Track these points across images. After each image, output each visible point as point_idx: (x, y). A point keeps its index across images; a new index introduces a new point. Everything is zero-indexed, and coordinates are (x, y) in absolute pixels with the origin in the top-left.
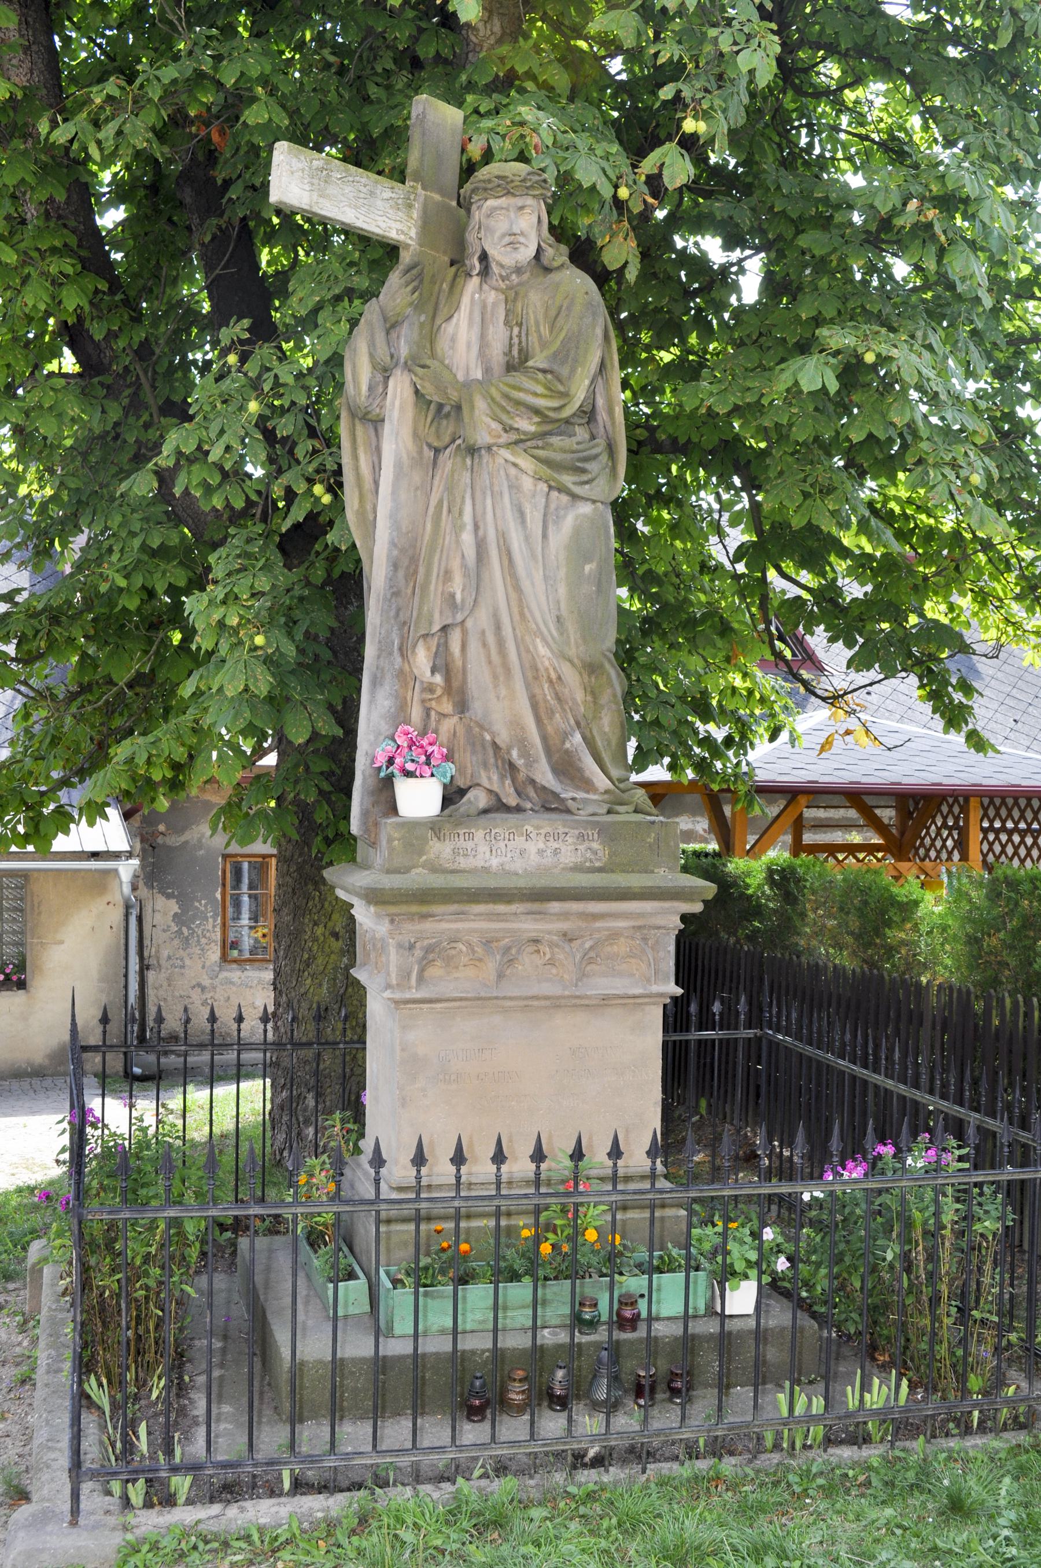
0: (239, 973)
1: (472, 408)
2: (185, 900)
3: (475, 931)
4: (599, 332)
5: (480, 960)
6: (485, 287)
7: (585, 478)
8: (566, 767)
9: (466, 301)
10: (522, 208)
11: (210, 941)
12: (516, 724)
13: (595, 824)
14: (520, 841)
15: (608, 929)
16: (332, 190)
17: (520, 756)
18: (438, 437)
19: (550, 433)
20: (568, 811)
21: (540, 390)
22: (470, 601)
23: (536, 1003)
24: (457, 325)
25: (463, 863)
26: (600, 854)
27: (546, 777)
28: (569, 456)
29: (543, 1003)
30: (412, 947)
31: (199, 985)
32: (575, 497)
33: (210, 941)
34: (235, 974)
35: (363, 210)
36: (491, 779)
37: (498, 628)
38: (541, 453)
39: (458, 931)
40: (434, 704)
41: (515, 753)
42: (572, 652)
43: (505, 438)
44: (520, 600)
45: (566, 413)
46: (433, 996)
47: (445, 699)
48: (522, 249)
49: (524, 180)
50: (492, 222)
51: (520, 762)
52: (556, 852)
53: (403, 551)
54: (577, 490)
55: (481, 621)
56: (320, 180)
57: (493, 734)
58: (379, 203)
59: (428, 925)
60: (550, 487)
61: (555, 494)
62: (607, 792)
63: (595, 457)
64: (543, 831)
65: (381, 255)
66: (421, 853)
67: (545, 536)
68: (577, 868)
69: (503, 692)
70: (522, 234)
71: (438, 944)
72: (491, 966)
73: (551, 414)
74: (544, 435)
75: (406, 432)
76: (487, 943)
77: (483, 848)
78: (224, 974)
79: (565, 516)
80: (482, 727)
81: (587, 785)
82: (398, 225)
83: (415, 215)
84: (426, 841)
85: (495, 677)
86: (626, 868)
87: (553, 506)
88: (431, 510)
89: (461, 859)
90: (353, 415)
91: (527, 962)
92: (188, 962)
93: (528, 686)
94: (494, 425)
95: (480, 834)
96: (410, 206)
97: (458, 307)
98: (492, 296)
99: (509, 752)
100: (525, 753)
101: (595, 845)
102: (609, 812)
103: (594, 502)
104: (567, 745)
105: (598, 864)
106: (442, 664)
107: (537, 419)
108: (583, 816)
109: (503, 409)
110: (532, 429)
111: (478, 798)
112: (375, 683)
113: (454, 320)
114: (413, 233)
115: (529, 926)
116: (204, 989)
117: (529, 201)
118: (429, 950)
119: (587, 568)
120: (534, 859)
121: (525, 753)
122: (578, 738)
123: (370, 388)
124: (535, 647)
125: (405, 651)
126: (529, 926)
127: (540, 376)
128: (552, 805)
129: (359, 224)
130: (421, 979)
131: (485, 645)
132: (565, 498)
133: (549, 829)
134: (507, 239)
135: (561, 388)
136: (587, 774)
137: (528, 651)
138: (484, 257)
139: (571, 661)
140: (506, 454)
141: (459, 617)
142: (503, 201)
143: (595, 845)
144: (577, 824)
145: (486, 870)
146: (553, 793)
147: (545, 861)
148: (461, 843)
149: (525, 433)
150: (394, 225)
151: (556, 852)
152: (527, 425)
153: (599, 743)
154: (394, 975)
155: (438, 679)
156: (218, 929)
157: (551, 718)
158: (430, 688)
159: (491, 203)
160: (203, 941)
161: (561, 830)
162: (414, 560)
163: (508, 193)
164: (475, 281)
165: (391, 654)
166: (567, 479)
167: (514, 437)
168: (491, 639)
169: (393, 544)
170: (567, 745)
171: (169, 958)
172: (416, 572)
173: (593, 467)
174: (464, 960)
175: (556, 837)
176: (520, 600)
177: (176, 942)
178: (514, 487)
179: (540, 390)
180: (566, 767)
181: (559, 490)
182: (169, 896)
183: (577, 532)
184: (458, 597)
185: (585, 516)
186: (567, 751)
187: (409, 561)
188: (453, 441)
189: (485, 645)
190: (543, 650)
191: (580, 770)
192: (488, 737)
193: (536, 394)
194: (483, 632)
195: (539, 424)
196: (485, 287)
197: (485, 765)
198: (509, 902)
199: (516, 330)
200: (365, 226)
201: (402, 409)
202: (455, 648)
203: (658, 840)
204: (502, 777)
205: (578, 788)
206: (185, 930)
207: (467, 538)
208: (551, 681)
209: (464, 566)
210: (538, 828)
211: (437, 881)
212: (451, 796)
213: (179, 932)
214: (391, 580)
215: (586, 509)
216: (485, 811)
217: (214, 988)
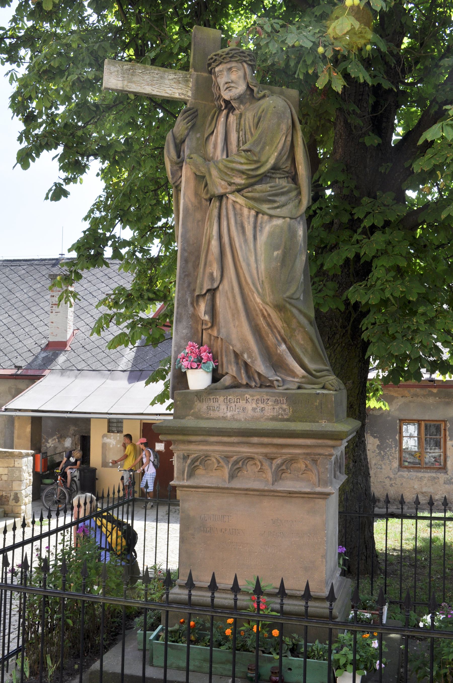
0: (407, 473)
2: (382, 439)
7: (276, 205)
10: (230, 69)
11: (394, 458)
12: (243, 340)
14: (243, 403)
15: (290, 454)
16: (135, 79)
21: (243, 160)
25: (213, 414)
26: (287, 411)
27: (260, 367)
31: (389, 477)
33: (394, 458)
34: (405, 473)
35: (156, 86)
38: (249, 194)
39: (207, 451)
41: (245, 356)
43: (229, 189)
48: (234, 90)
51: (249, 361)
52: (262, 409)
54: (272, 212)
55: (225, 286)
56: (129, 75)
58: (167, 82)
59: (192, 447)
62: (303, 377)
65: (170, 105)
66: (191, 408)
68: (274, 419)
70: (232, 82)
77: (223, 407)
78: (400, 473)
81: (293, 374)
82: (180, 91)
83: (191, 85)
86: (301, 420)
87: (259, 222)
89: (212, 412)
91: (250, 469)
92: (383, 467)
94: (223, 183)
95: (221, 399)
96: (187, 81)
99: (242, 355)
100: (250, 356)
101: (285, 406)
102: (299, 388)
103: (284, 218)
105: (285, 417)
107: (245, 177)
109: (226, 174)
110: (243, 182)
111: (227, 380)
114: (190, 94)
115: (245, 450)
116: (391, 479)
117: (234, 64)
119: (275, 253)
120: (250, 413)
121: (250, 356)
122: (284, 347)
124: (254, 299)
126: (245, 450)
128: (265, 384)
129: (154, 93)
132: (266, 217)
133: (258, 397)
135: (255, 158)
140: (230, 196)
143: (285, 406)
144: (274, 395)
145: (224, 418)
147: (256, 414)
148: (211, 404)
150: (176, 91)
151: (262, 409)
152: (240, 180)
155: (207, 318)
156: (397, 452)
160: (391, 457)
161: (265, 397)
165: (186, 306)
166: (265, 207)
167: (234, 188)
168: (230, 295)
171: (375, 464)
175: (263, 402)
177: (378, 457)
179: (243, 160)
180: (277, 364)
182: (375, 437)
183: (271, 235)
184: (215, 274)
185: (276, 226)
192: (231, 348)
193: (241, 163)
195: (247, 179)
198: (230, 436)
200: (158, 94)
203: (321, 404)
206: (382, 452)
210: (252, 396)
212: (216, 377)
213: (380, 453)
215: (279, 222)
217: (395, 479)
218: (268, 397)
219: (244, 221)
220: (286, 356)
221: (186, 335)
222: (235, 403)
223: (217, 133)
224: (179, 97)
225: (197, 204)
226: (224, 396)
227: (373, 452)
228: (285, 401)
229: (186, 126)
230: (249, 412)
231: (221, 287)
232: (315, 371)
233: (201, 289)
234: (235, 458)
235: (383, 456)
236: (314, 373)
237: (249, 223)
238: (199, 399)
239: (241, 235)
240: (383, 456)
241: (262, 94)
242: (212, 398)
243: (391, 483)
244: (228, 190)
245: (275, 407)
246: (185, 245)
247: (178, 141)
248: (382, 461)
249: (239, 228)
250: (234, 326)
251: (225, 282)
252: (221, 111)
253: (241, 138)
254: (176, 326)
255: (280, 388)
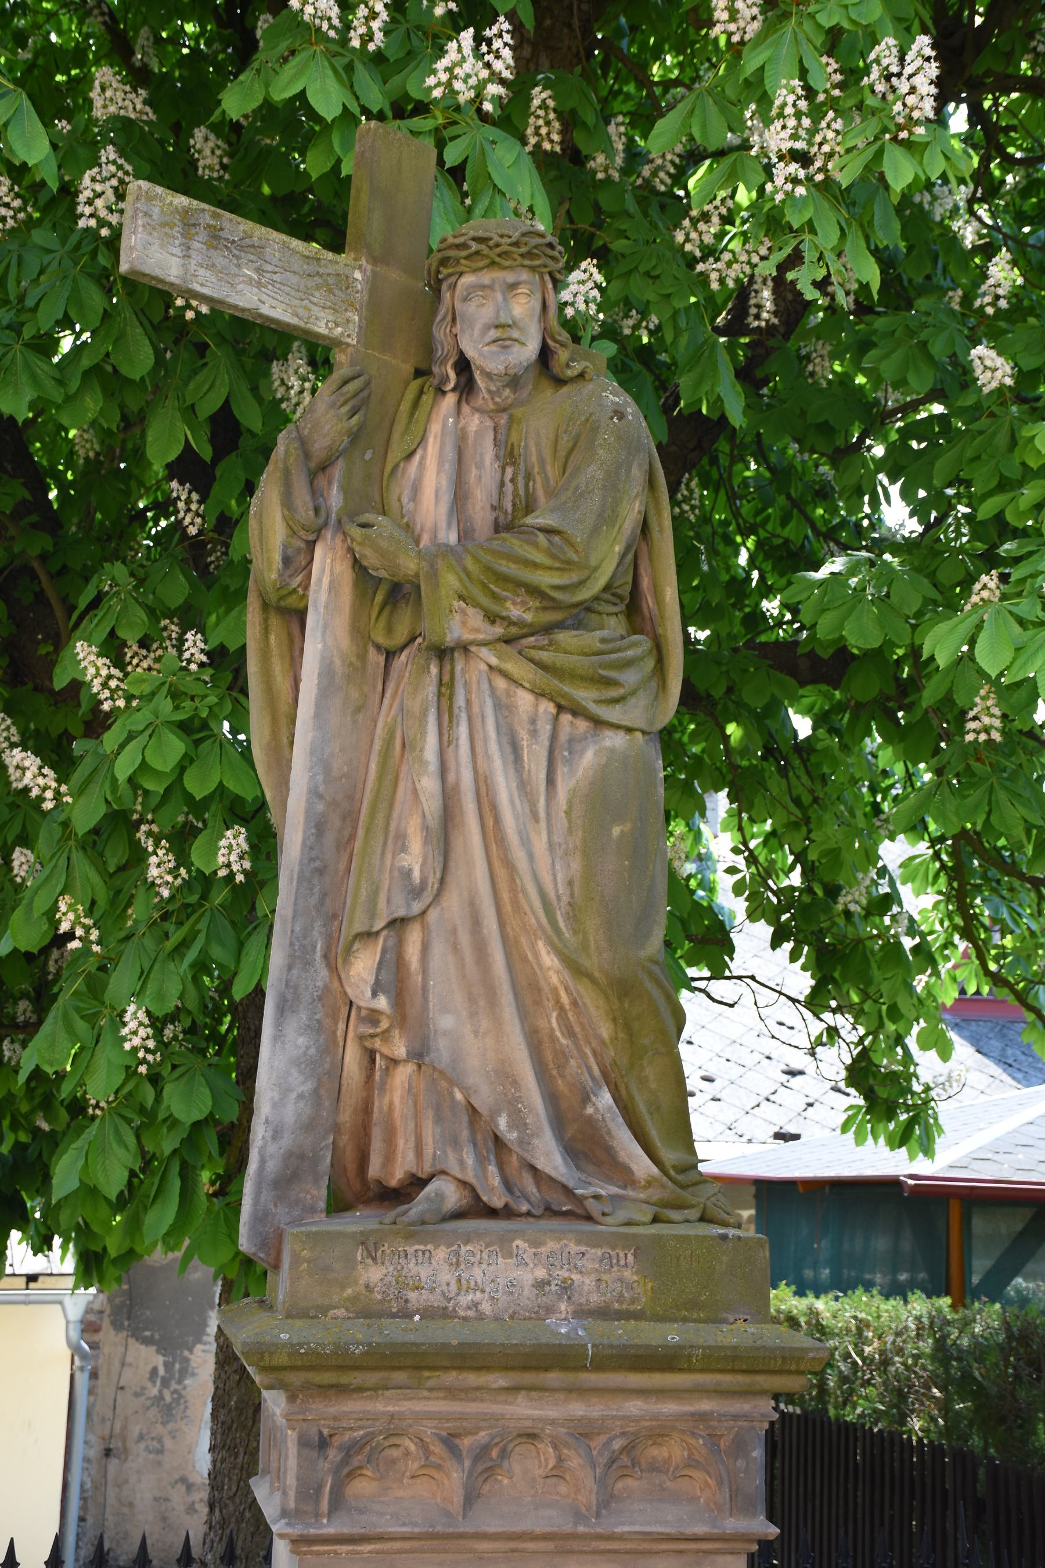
1: (436, 586)
3: (430, 1416)
4: (638, 474)
5: (439, 1467)
6: (466, 409)
7: (614, 693)
8: (586, 1146)
9: (435, 428)
10: (513, 286)
12: (505, 1075)
13: (627, 1241)
17: (511, 1126)
18: (390, 630)
19: (560, 626)
20: (589, 1218)
22: (433, 881)
23: (531, 1546)
24: (422, 465)
27: (551, 1159)
28: (586, 661)
29: (542, 1545)
30: (323, 1444)
31: (183, 1480)
32: (598, 723)
36: (465, 1162)
37: (476, 922)
38: (544, 656)
40: (377, 1044)
41: (502, 1122)
42: (590, 963)
44: (512, 880)
45: (584, 595)
46: (357, 1530)
47: (396, 1033)
48: (516, 348)
49: (516, 244)
50: (471, 308)
51: (511, 1136)
53: (334, 804)
57: (465, 1090)
59: (352, 1406)
60: (560, 708)
61: (566, 718)
62: (650, 1183)
63: (629, 663)
64: (544, 1250)
67: (551, 781)
69: (485, 1024)
71: (369, 1438)
72: (455, 1478)
73: (555, 595)
74: (548, 629)
75: (342, 623)
76: (450, 1442)
77: (446, 1276)
79: (583, 751)
80: (452, 1083)
81: (623, 1174)
84: (351, 1264)
85: (471, 999)
88: (377, 747)
89: (412, 1296)
90: (265, 606)
91: (527, 1467)
93: (523, 1015)
95: (441, 1253)
97: (423, 440)
98: (474, 422)
100: (518, 1122)
101: (627, 1274)
102: (655, 1220)
103: (629, 730)
104: (590, 1110)
106: (394, 978)
108: (149, 1385)
112: (282, 1010)
113: (417, 458)
114: (354, 329)
115: (524, 1410)
118: (350, 1450)
121: (518, 1122)
122: (605, 1099)
123: (287, 561)
124: (537, 955)
125: (336, 962)
127: (542, 538)
128: (565, 1209)
130: (337, 1502)
131: (455, 948)
132: (582, 725)
134: (493, 334)
136: (622, 1157)
137: (524, 959)
138: (463, 365)
139: (593, 981)
140: (484, 652)
141: (417, 907)
142: (486, 277)
144: (594, 1241)
146: (565, 1188)
149: (519, 623)
153: (642, 1107)
154: (292, 1494)
155: (382, 1003)
157: (561, 1067)
158: (373, 1017)
159: (467, 280)
161: (574, 1248)
162: (351, 817)
163: (493, 264)
164: (451, 399)
165: (308, 964)
166: (585, 696)
167: (498, 630)
168: (465, 939)
169: (314, 793)
170: (590, 1110)
171: (141, 1438)
172: (352, 837)
173: (630, 677)
174: (413, 1466)
176: (512, 880)
178: (503, 708)
180: (586, 1146)
181: (575, 713)
182: (147, 1342)
184: (416, 874)
185: (612, 750)
186: (590, 1121)
187: (346, 820)
188: (413, 639)
189: (455, 948)
190: (549, 960)
191: (609, 1151)
192: (459, 1096)
194: (454, 931)
196: (466, 409)
197: (455, 1143)
199: (509, 471)
201: (333, 588)
202: (412, 952)
204: (481, 1161)
205: (609, 1180)
207: (429, 784)
208: (562, 1009)
209: (426, 828)
210: (535, 1243)
211: (359, 1334)
214: (307, 847)
215: (615, 740)
216: (458, 1215)
218: (583, 1249)
219: (518, 728)
220: (612, 1126)
221: (305, 1054)
222: (484, 1266)
223: (423, 458)
224: (326, 332)
225: (354, 659)
226: (449, 1246)
227: (136, 1395)
228: (631, 1258)
229: (345, 425)
230: (526, 1293)
231: (432, 916)
232: (674, 1167)
233: (372, 915)
234: (483, 1436)
235: (169, 1407)
236: (672, 1173)
237: (534, 733)
238: (370, 1255)
239: (511, 766)
240: (169, 1407)
241: (577, 367)
242: (410, 1250)
243: (190, 1499)
244: (481, 637)
245: (605, 1277)
246: (320, 778)
247: (313, 465)
248: (164, 1424)
249: (508, 749)
250: (476, 1033)
251: (453, 902)
252: (441, 392)
253: (509, 487)
254: (279, 1024)
255: (608, 1220)
